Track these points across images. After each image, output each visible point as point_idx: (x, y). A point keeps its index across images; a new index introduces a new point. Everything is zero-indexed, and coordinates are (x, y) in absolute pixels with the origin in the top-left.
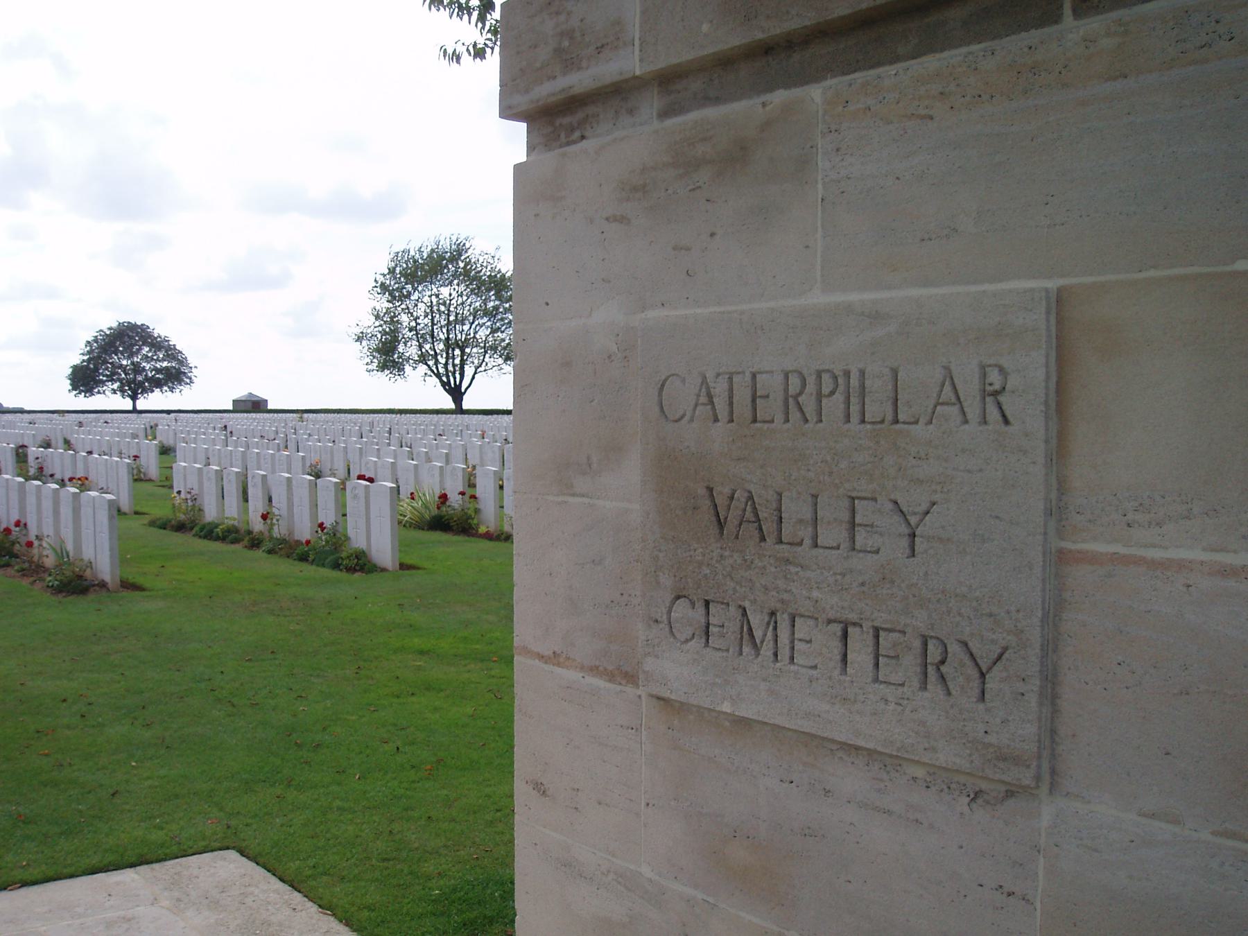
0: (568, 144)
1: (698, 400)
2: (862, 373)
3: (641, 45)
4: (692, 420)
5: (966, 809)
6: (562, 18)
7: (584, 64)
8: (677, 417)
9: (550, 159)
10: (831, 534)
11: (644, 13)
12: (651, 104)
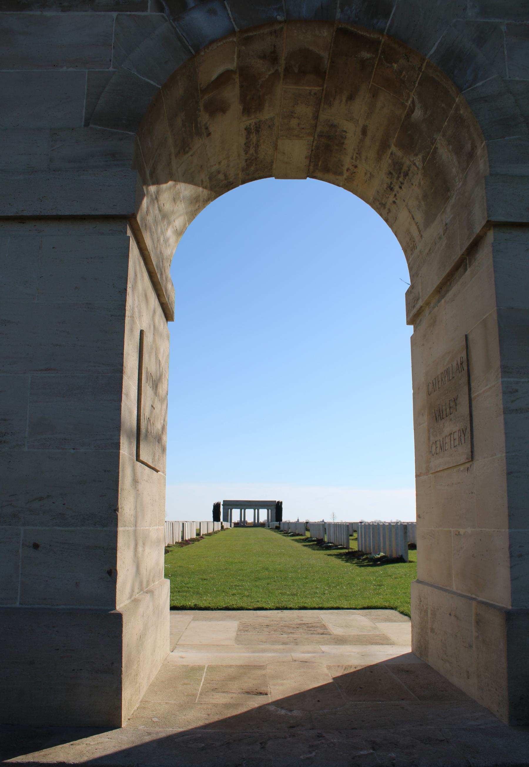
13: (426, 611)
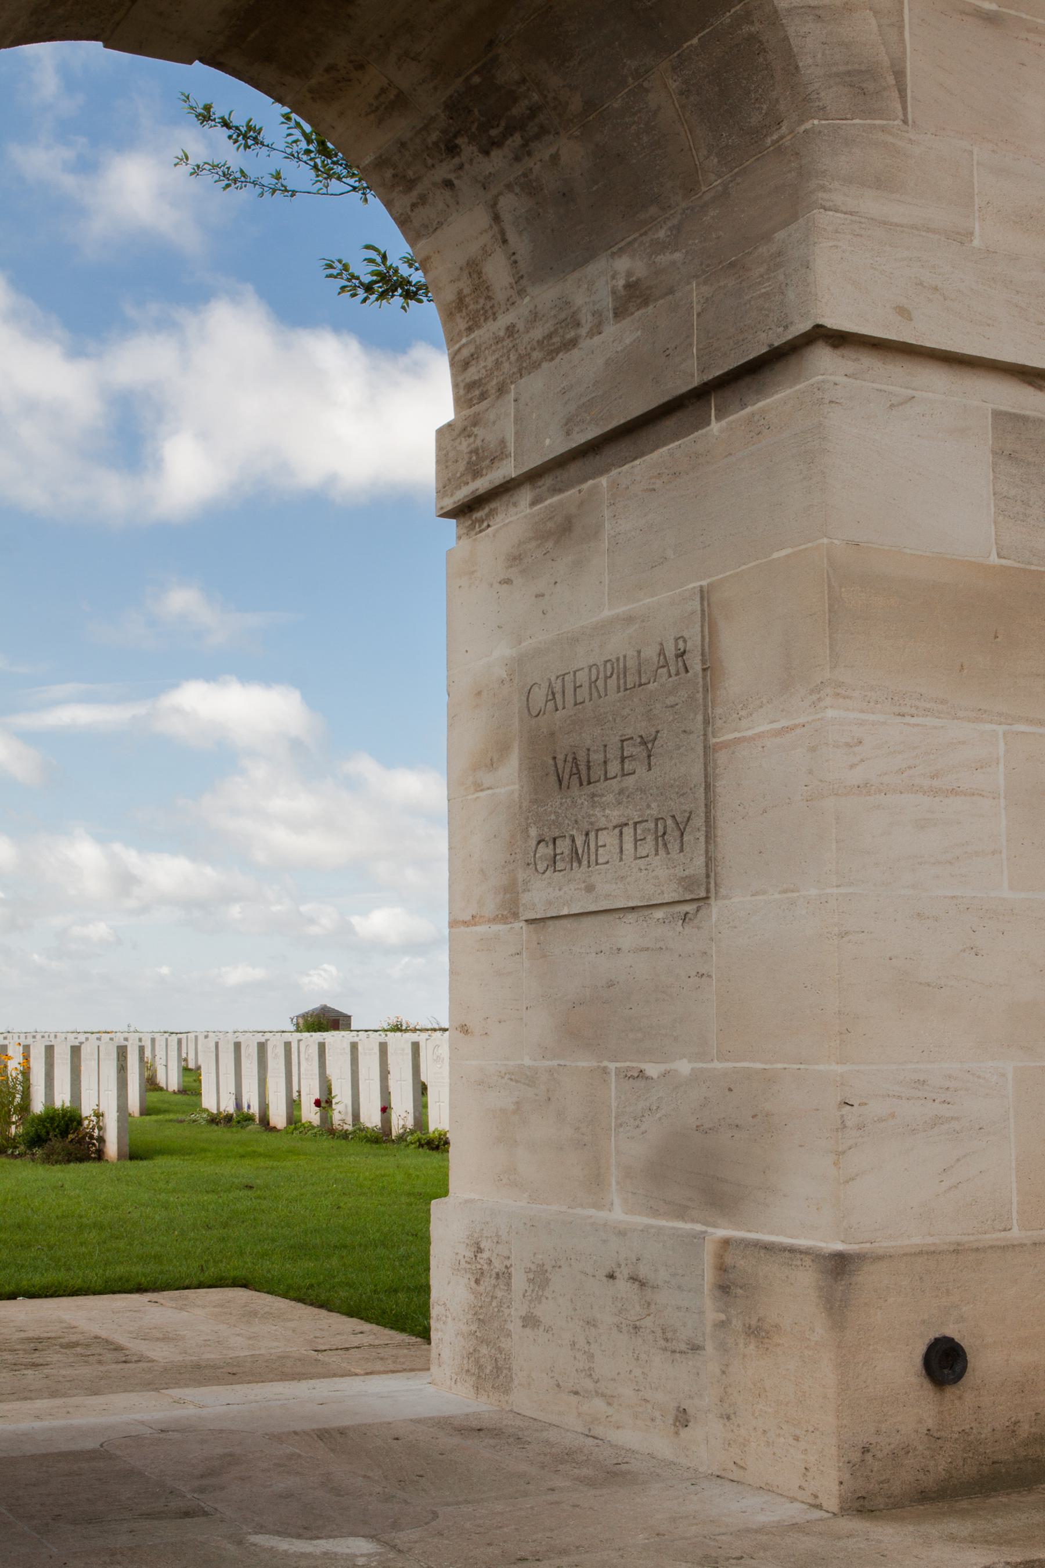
0: (481, 531)
1: (547, 698)
2: (625, 657)
3: (515, 456)
4: (544, 713)
5: (680, 929)
6: (472, 439)
7: (484, 472)
8: (537, 713)
9: (466, 542)
10: (614, 768)
11: (516, 433)
12: (525, 496)
13: (504, 1276)
